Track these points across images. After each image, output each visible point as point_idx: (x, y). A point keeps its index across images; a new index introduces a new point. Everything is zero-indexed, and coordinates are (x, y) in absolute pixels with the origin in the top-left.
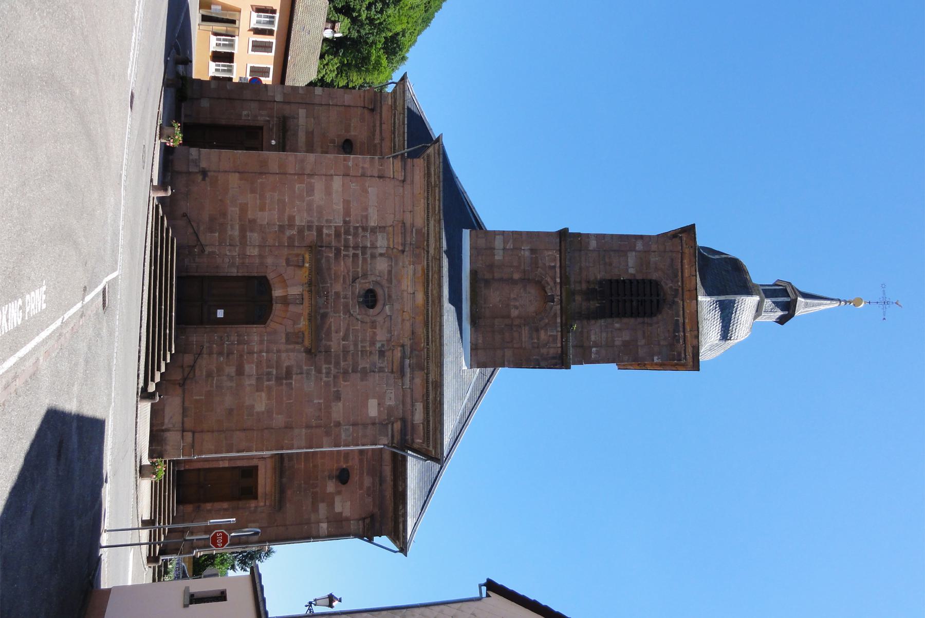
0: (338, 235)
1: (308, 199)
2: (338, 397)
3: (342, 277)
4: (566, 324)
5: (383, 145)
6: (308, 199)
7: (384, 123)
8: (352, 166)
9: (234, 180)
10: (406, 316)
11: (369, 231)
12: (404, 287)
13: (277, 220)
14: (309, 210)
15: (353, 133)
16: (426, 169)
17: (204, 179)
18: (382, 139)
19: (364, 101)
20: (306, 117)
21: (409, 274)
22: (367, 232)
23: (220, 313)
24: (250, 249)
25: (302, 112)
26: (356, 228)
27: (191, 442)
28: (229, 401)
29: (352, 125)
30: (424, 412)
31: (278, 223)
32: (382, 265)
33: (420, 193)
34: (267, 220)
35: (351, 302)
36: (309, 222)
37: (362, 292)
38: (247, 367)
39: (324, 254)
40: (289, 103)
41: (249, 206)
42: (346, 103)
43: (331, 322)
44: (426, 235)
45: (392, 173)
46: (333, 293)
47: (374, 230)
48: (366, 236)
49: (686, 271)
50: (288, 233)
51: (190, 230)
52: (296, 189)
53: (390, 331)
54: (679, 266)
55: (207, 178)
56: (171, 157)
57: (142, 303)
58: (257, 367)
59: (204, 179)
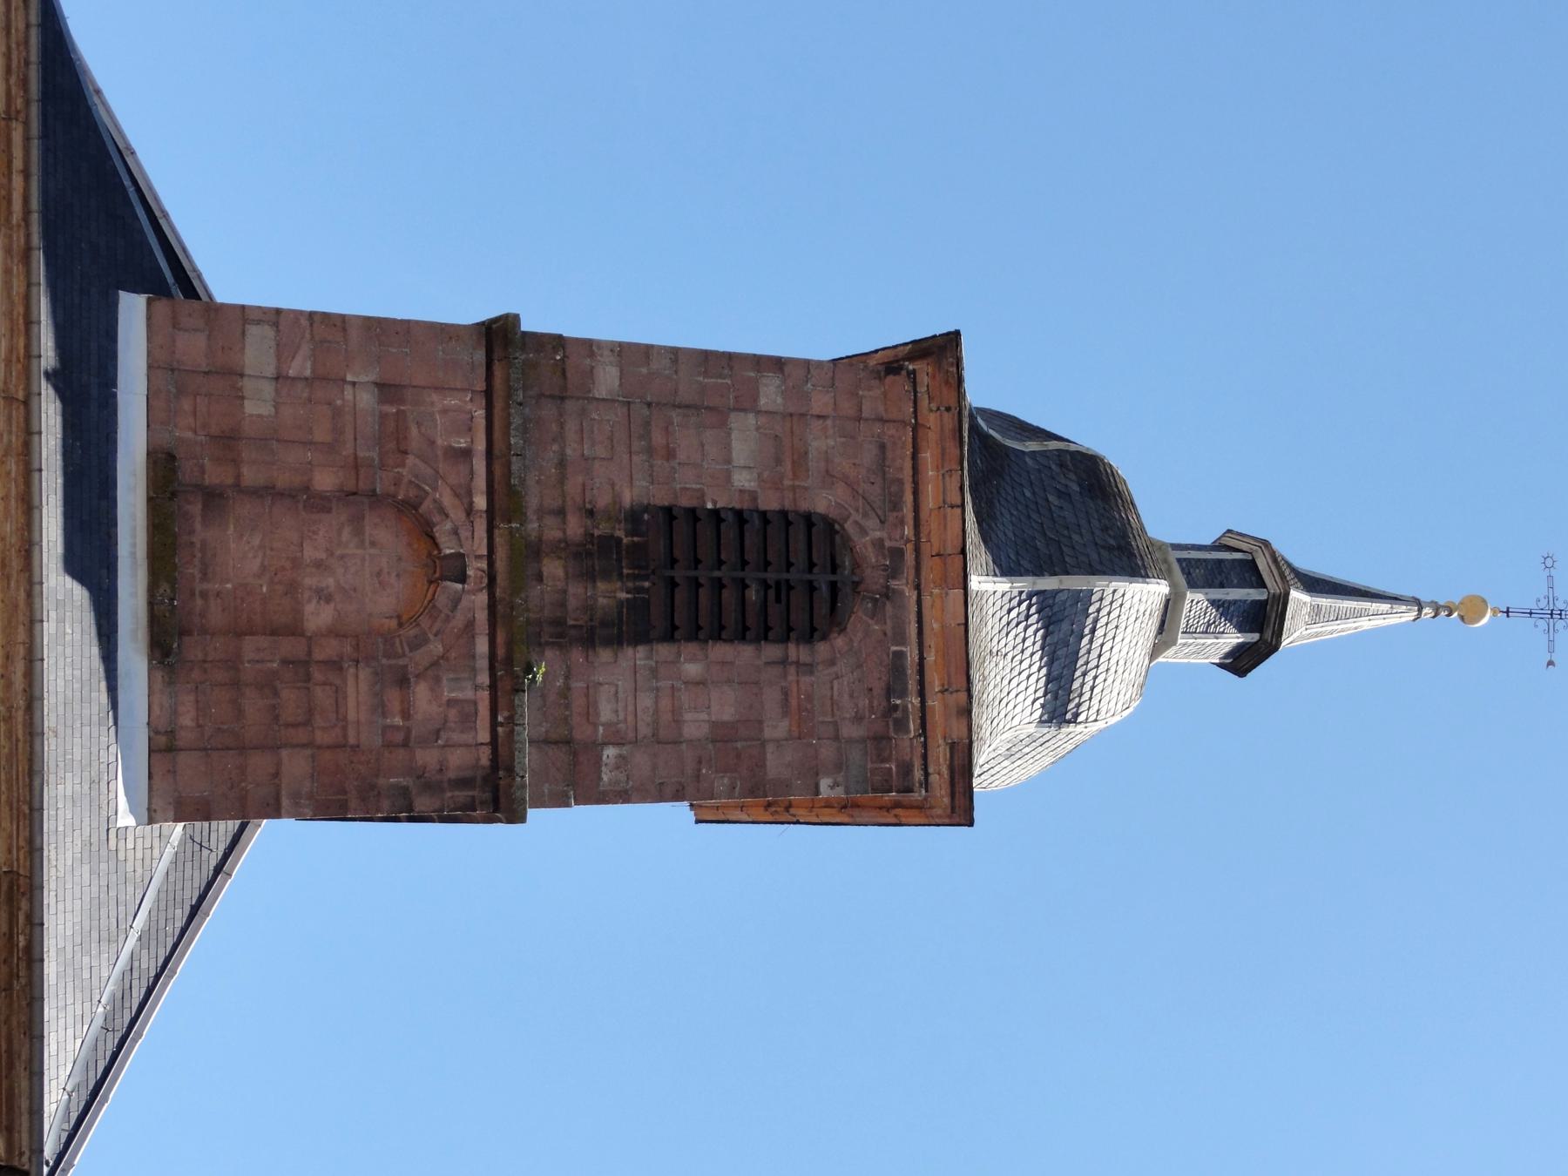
54: (908, 471)
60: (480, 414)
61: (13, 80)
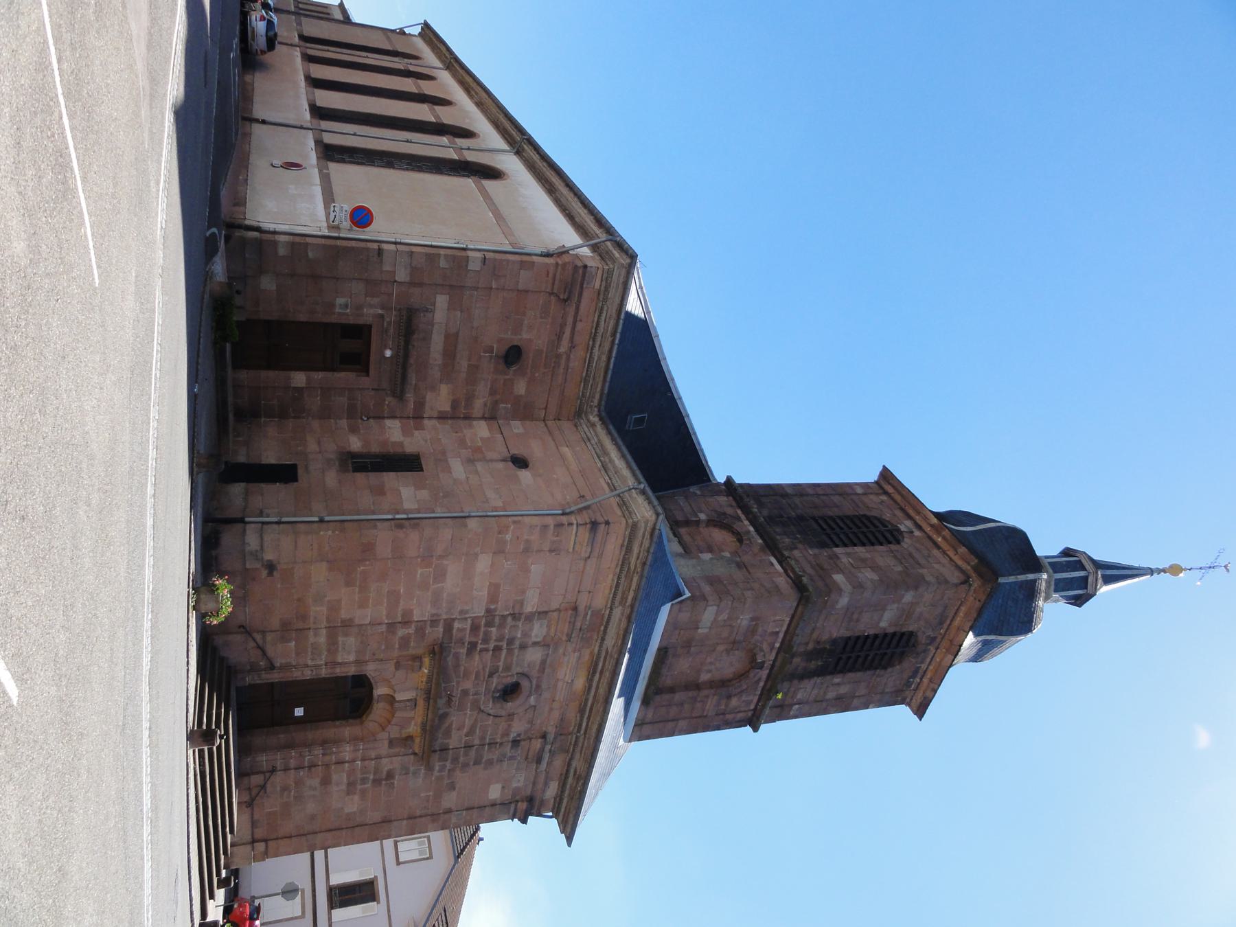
0: (475, 628)
1: (436, 586)
2: (452, 787)
3: (474, 673)
4: (769, 690)
5: (572, 356)
6: (436, 586)
7: (581, 321)
8: (511, 540)
9: (320, 573)
10: (556, 705)
11: (522, 620)
12: (560, 674)
13: (384, 618)
14: (436, 600)
15: (525, 336)
16: (627, 540)
17: (270, 574)
18: (572, 347)
19: (553, 284)
20: (448, 310)
21: (571, 661)
22: (520, 621)
23: (299, 712)
24: (342, 655)
25: (442, 301)
26: (504, 617)
27: (247, 222)
28: (311, 807)
29: (526, 322)
30: (558, 789)
31: (386, 622)
32: (534, 656)
33: (609, 568)
34: (369, 618)
35: (483, 698)
36: (433, 615)
37: (500, 687)
38: (335, 777)
39: (452, 650)
40: (421, 285)
41: (343, 602)
42: (520, 287)
43: (452, 721)
44: (605, 620)
45: (572, 543)
46: (459, 692)
47: (530, 618)
48: (518, 626)
49: (959, 619)
50: (401, 632)
51: (252, 644)
52: (418, 576)
53: (531, 722)
54: (952, 614)
55: (275, 573)
56: (214, 553)
57: (188, 809)
58: (349, 776)
59: (270, 574)
60: (788, 620)
61: (639, 561)
